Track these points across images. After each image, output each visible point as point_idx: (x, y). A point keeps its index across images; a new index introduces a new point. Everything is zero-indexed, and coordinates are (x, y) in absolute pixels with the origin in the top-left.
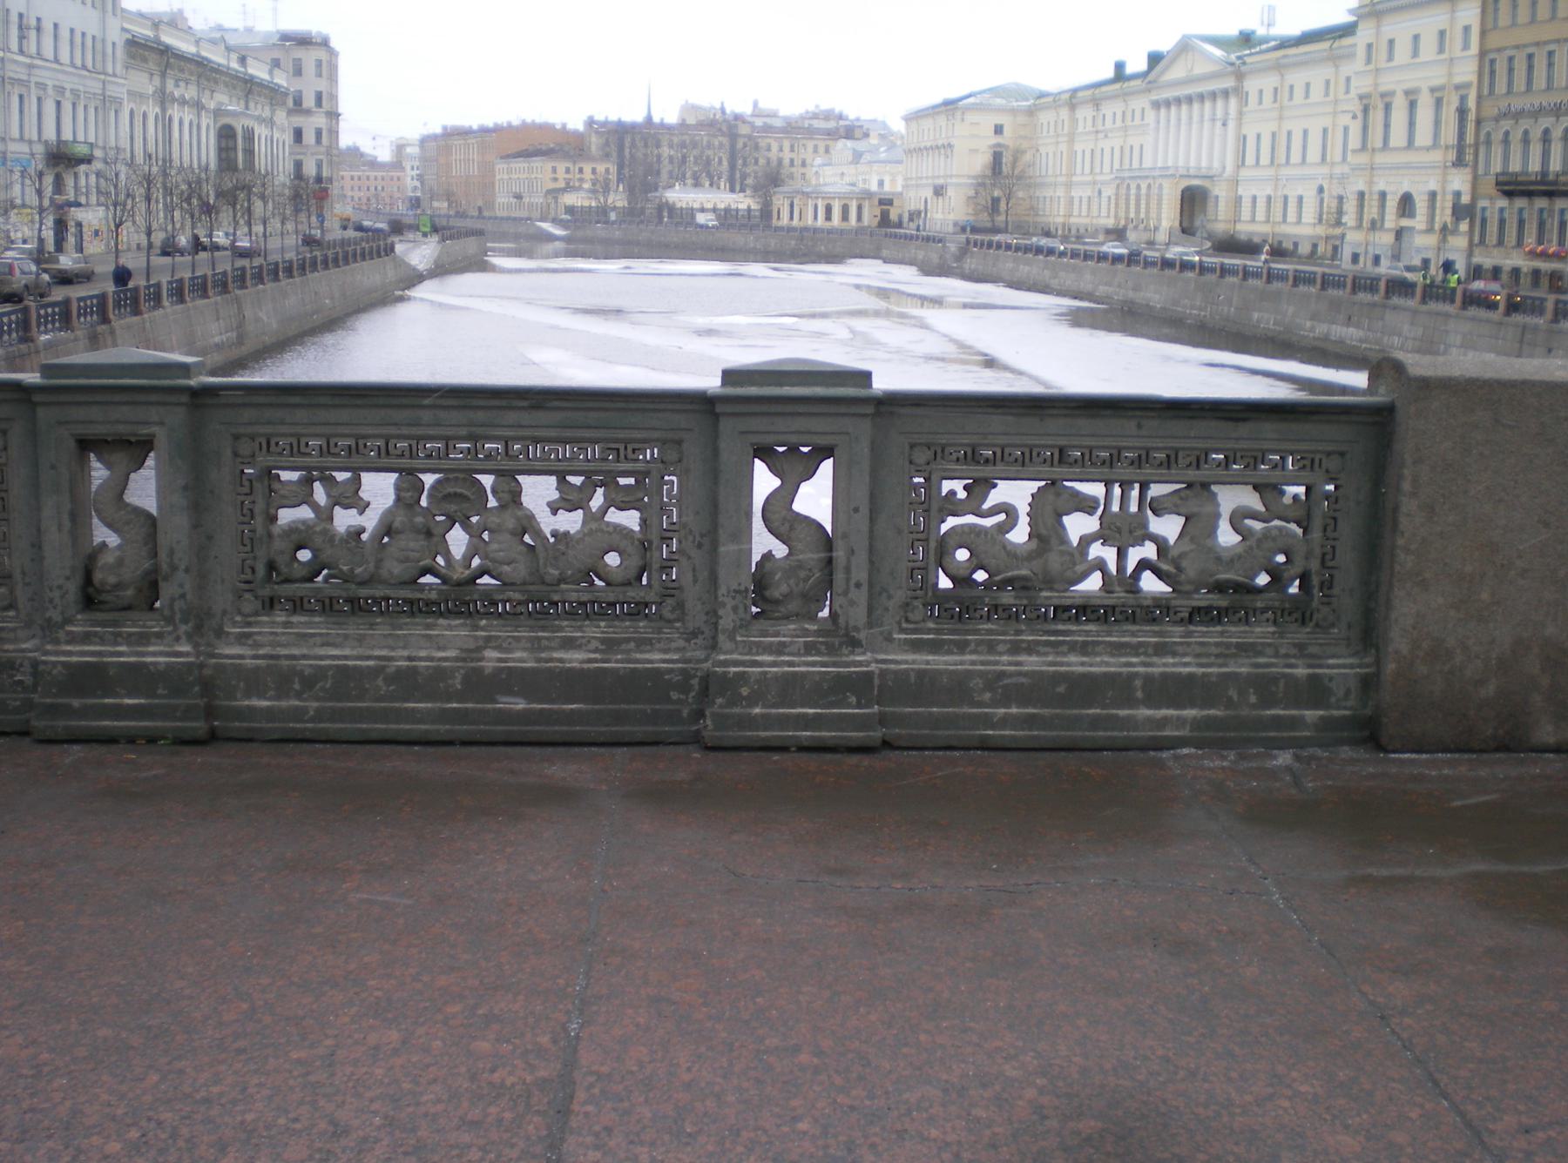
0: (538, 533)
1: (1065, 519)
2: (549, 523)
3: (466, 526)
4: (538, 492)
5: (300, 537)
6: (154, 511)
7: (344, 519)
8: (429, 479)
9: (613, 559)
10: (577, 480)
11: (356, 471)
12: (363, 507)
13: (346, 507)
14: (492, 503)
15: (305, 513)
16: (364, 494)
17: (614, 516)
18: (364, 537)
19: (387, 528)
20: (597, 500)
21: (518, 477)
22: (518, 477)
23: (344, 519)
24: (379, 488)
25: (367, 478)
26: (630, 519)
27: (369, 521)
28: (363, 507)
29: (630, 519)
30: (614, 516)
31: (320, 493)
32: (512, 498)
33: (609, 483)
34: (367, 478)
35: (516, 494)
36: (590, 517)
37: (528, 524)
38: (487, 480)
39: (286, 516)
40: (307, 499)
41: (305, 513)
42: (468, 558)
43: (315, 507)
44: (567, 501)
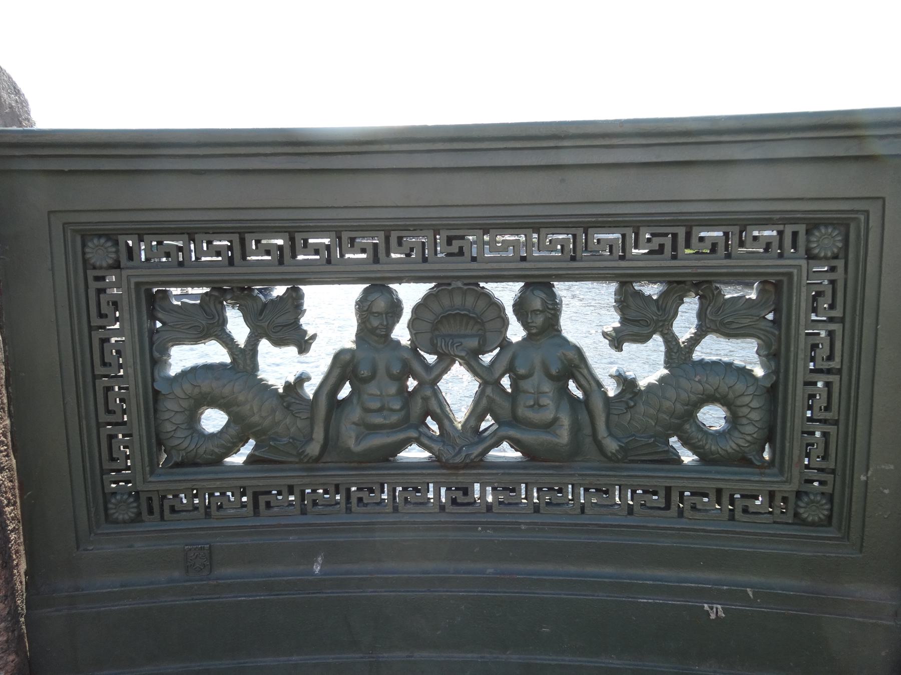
0: (591, 384)
1: (613, 287)
2: (606, 364)
3: (474, 367)
4: (586, 313)
5: (204, 386)
6: (523, 284)
7: (277, 365)
8: (411, 294)
9: (713, 417)
10: (652, 290)
11: (297, 280)
12: (303, 344)
13: (278, 342)
14: (516, 332)
15: (213, 353)
16: (308, 322)
17: (714, 349)
18: (309, 390)
19: (344, 366)
20: (685, 323)
21: (394, 286)
22: (394, 286)
23: (277, 365)
24: (331, 313)
25: (311, 293)
26: (744, 353)
27: (316, 365)
28: (303, 344)
29: (744, 353)
30: (714, 349)
31: (237, 326)
32: (543, 317)
33: (704, 286)
34: (311, 293)
35: (553, 309)
36: (678, 355)
37: (574, 364)
38: (506, 293)
39: (183, 357)
40: (214, 329)
41: (213, 353)
42: (477, 414)
43: (227, 341)
44: (638, 321)
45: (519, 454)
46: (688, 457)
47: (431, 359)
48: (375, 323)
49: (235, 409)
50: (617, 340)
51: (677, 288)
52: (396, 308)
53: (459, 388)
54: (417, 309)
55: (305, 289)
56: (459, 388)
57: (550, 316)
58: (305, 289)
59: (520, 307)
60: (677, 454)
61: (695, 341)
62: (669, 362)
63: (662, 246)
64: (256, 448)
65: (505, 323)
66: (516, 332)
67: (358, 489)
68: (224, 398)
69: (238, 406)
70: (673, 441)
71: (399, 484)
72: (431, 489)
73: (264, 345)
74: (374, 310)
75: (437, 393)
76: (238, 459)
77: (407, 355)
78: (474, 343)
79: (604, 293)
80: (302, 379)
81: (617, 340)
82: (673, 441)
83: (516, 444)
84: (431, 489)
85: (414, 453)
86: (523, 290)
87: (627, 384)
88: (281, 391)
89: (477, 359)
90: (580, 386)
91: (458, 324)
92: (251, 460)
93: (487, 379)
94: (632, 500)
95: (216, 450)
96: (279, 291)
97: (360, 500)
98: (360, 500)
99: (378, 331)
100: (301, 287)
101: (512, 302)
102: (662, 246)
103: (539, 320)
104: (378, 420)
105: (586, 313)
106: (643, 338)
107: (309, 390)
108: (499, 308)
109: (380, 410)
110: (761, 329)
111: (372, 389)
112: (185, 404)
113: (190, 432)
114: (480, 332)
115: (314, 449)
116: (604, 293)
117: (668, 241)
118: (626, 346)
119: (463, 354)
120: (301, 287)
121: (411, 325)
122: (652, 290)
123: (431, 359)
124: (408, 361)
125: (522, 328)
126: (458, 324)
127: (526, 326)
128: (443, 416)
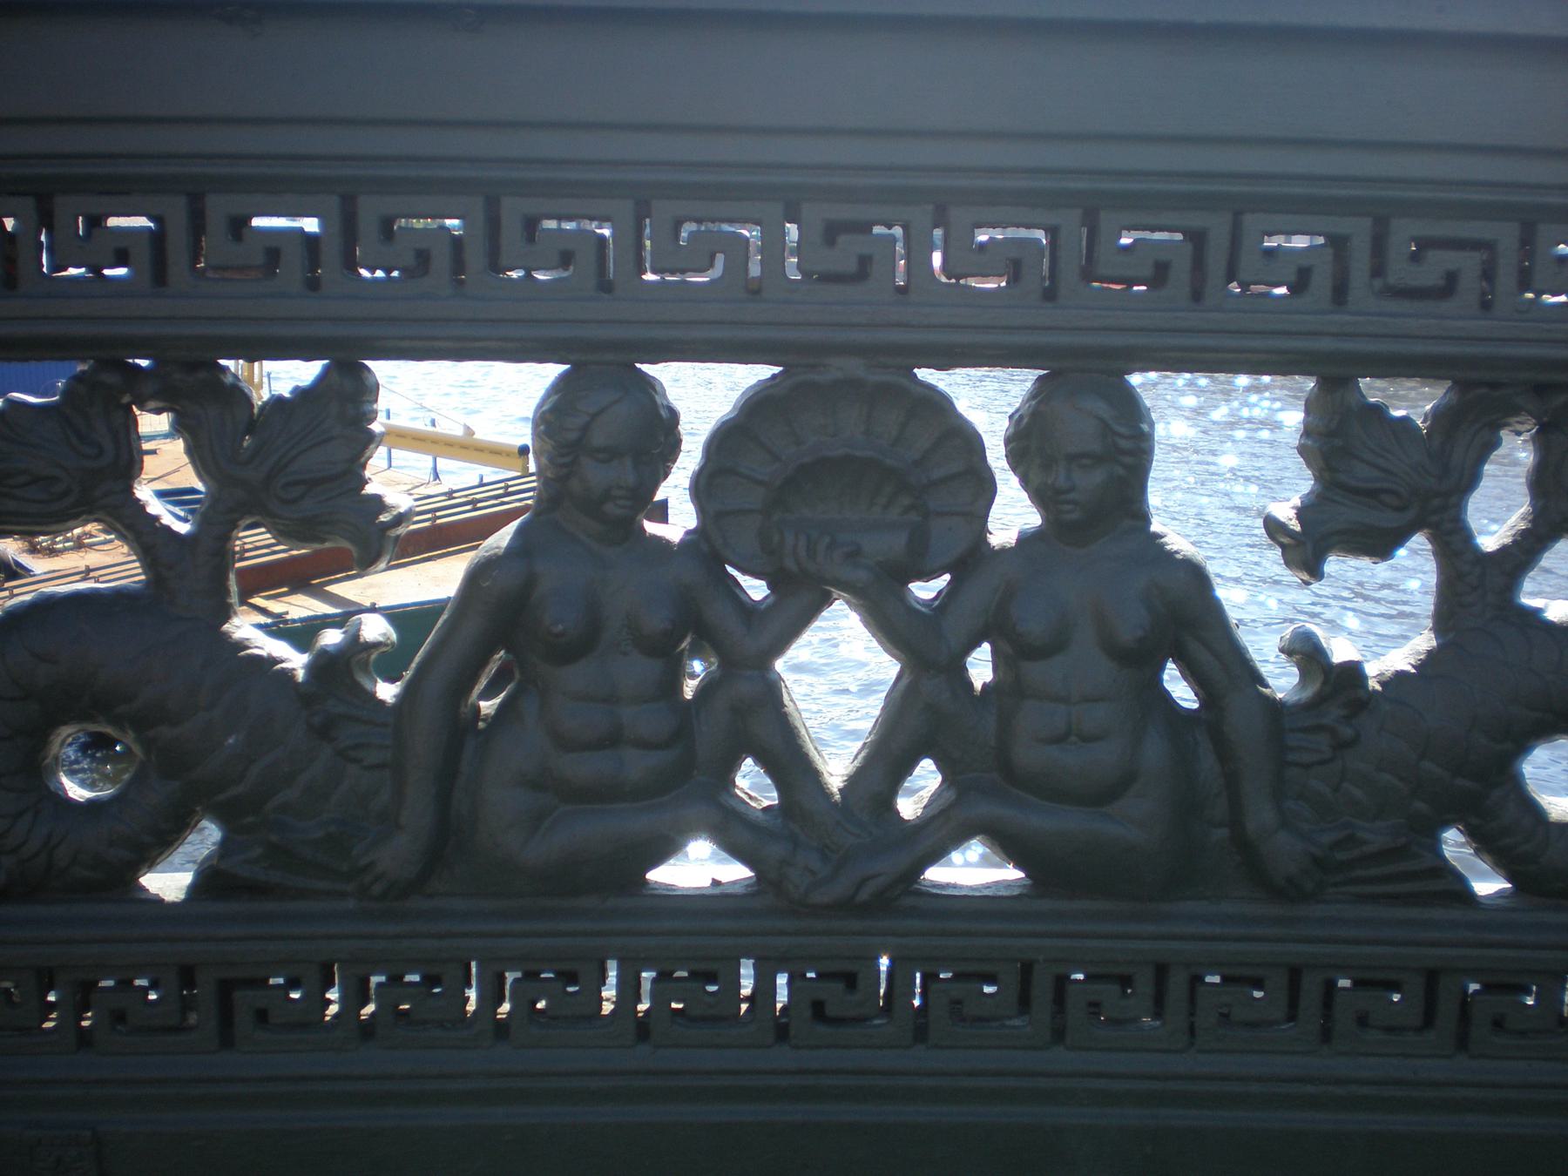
2: (1261, 608)
3: (893, 623)
4: (1221, 462)
8: (704, 395)
10: (1413, 403)
14: (1012, 515)
15: (92, 560)
19: (499, 614)
32: (1094, 470)
35: (1127, 450)
36: (1477, 592)
37: (1184, 612)
38: (987, 400)
42: (887, 761)
45: (1012, 873)
46: (1488, 885)
47: (756, 589)
48: (596, 475)
50: (1305, 548)
52: (660, 433)
53: (837, 679)
54: (725, 440)
55: (381, 369)
56: (837, 679)
57: (1120, 471)
58: (381, 369)
59: (1027, 442)
60: (1461, 880)
62: (1447, 616)
63: (1452, 279)
64: (225, 847)
65: (986, 488)
66: (1012, 515)
67: (958, 977)
70: (1454, 844)
71: (512, 962)
72: (612, 975)
75: (772, 692)
76: (167, 883)
78: (893, 544)
79: (1275, 410)
81: (1305, 548)
82: (1454, 844)
83: (1009, 846)
84: (612, 975)
85: (698, 868)
86: (1040, 392)
87: (1336, 684)
89: (902, 595)
90: (1193, 674)
91: (843, 490)
92: (209, 883)
93: (922, 645)
94: (7, 990)
96: (284, 377)
97: (1095, 1007)
98: (1095, 1007)
99: (609, 508)
100: (368, 363)
101: (1003, 425)
102: (1452, 279)
103: (1091, 480)
104: (582, 768)
105: (1221, 462)
106: (1380, 545)
108: (968, 441)
110: (1363, 461)
114: (914, 517)
115: (395, 855)
116: (1275, 410)
117: (1468, 264)
118: (1334, 565)
119: (861, 576)
120: (368, 363)
121: (701, 488)
122: (1413, 403)
123: (756, 589)
124: (690, 590)
125: (33, 364)
126: (843, 490)
127: (1040, 496)
128: (789, 761)
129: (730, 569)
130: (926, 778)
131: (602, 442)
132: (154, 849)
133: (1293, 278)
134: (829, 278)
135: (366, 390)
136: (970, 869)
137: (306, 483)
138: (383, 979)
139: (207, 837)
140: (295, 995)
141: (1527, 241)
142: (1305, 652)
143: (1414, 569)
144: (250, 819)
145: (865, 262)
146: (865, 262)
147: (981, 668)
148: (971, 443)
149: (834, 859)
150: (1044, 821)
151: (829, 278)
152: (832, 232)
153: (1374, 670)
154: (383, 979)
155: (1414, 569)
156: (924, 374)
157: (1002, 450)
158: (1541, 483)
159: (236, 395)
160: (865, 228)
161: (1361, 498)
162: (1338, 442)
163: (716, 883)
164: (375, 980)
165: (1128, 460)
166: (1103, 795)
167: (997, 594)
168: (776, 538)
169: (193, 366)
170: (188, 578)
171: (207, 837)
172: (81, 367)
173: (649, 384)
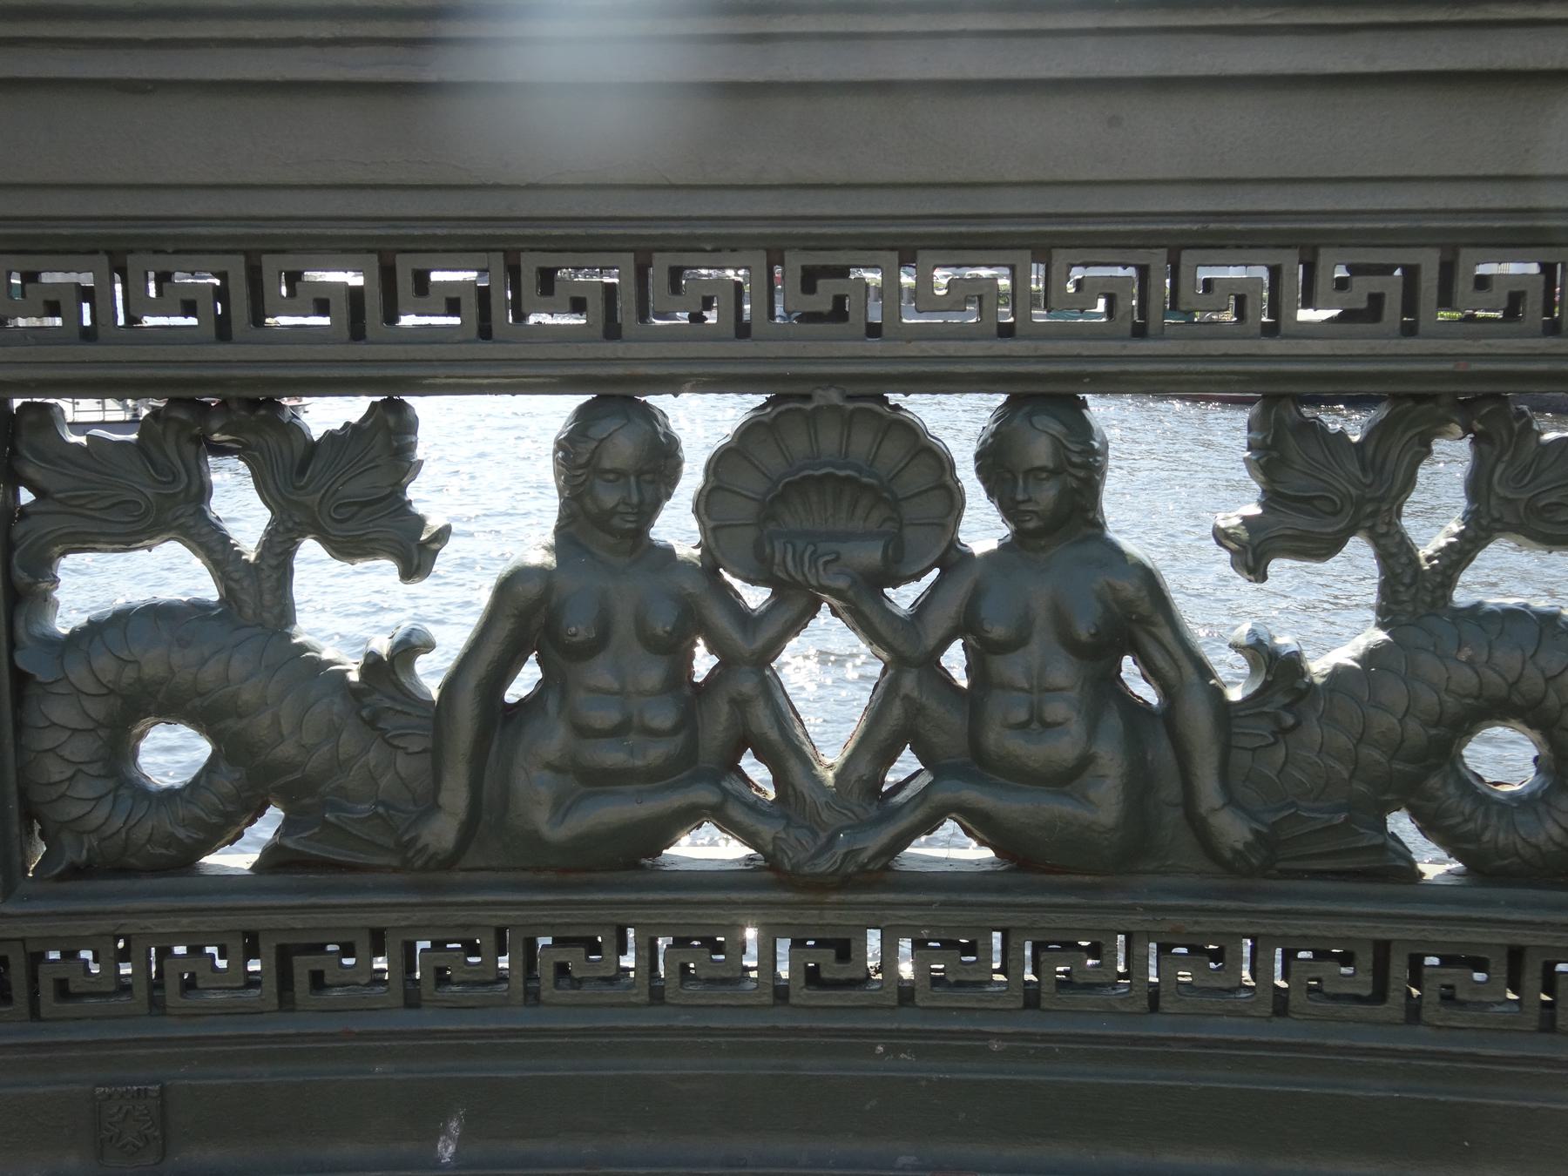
0: (1180, 664)
2: (1225, 614)
8: (702, 422)
13: (346, 547)
14: (982, 528)
15: (169, 573)
19: (522, 614)
32: (1055, 489)
35: (1082, 469)
36: (1412, 593)
37: (1138, 612)
38: (957, 422)
42: (876, 744)
46: (1434, 864)
47: (755, 597)
49: (232, 724)
50: (1252, 552)
51: (1415, 412)
52: (662, 459)
53: (827, 679)
54: (720, 463)
55: (421, 405)
56: (827, 679)
58: (421, 405)
59: (992, 461)
61: (1459, 555)
64: (286, 829)
65: (954, 501)
66: (982, 528)
68: (200, 695)
69: (240, 717)
70: (1401, 824)
73: (310, 551)
74: (607, 464)
75: (771, 690)
76: (235, 859)
77: (692, 586)
78: (870, 555)
79: (1226, 432)
80: (410, 647)
81: (1252, 552)
82: (1401, 824)
83: (980, 825)
85: (707, 847)
86: (1004, 416)
87: (1277, 667)
88: (354, 677)
90: (1151, 672)
92: (273, 859)
93: (905, 650)
95: (181, 833)
99: (616, 521)
100: (408, 400)
101: (974, 447)
104: (611, 756)
105: (1172, 482)
106: (1321, 547)
107: (430, 674)
109: (617, 732)
111: (599, 673)
112: (97, 709)
113: (111, 784)
114: (888, 526)
120: (408, 400)
121: (704, 505)
123: (755, 597)
126: (828, 499)
127: (1009, 510)
128: (786, 751)
129: (727, 577)
130: (907, 764)
131: (607, 479)
132: (225, 831)
133: (1505, 305)
134: (809, 317)
135: (407, 425)
136: (952, 848)
137: (362, 501)
138: (428, 944)
139: (266, 827)
140: (348, 961)
141: (1448, 272)
142: (1259, 652)
143: (1358, 561)
144: (307, 801)
145: (839, 301)
146: (839, 301)
147: (955, 660)
148: (941, 462)
149: (829, 857)
150: (1014, 806)
151: (809, 317)
152: (809, 280)
153: (1319, 666)
154: (428, 944)
155: (1358, 561)
156: (894, 398)
157: (971, 465)
158: (1477, 486)
159: (294, 430)
160: (843, 272)
161: (1303, 508)
162: (1275, 454)
163: (676, 395)
164: (423, 944)
165: (1082, 474)
166: (1068, 778)
167: (971, 594)
168: (768, 550)
169: (254, 404)
170: (258, 590)
171: (266, 827)
172: (161, 404)
173: (649, 414)
